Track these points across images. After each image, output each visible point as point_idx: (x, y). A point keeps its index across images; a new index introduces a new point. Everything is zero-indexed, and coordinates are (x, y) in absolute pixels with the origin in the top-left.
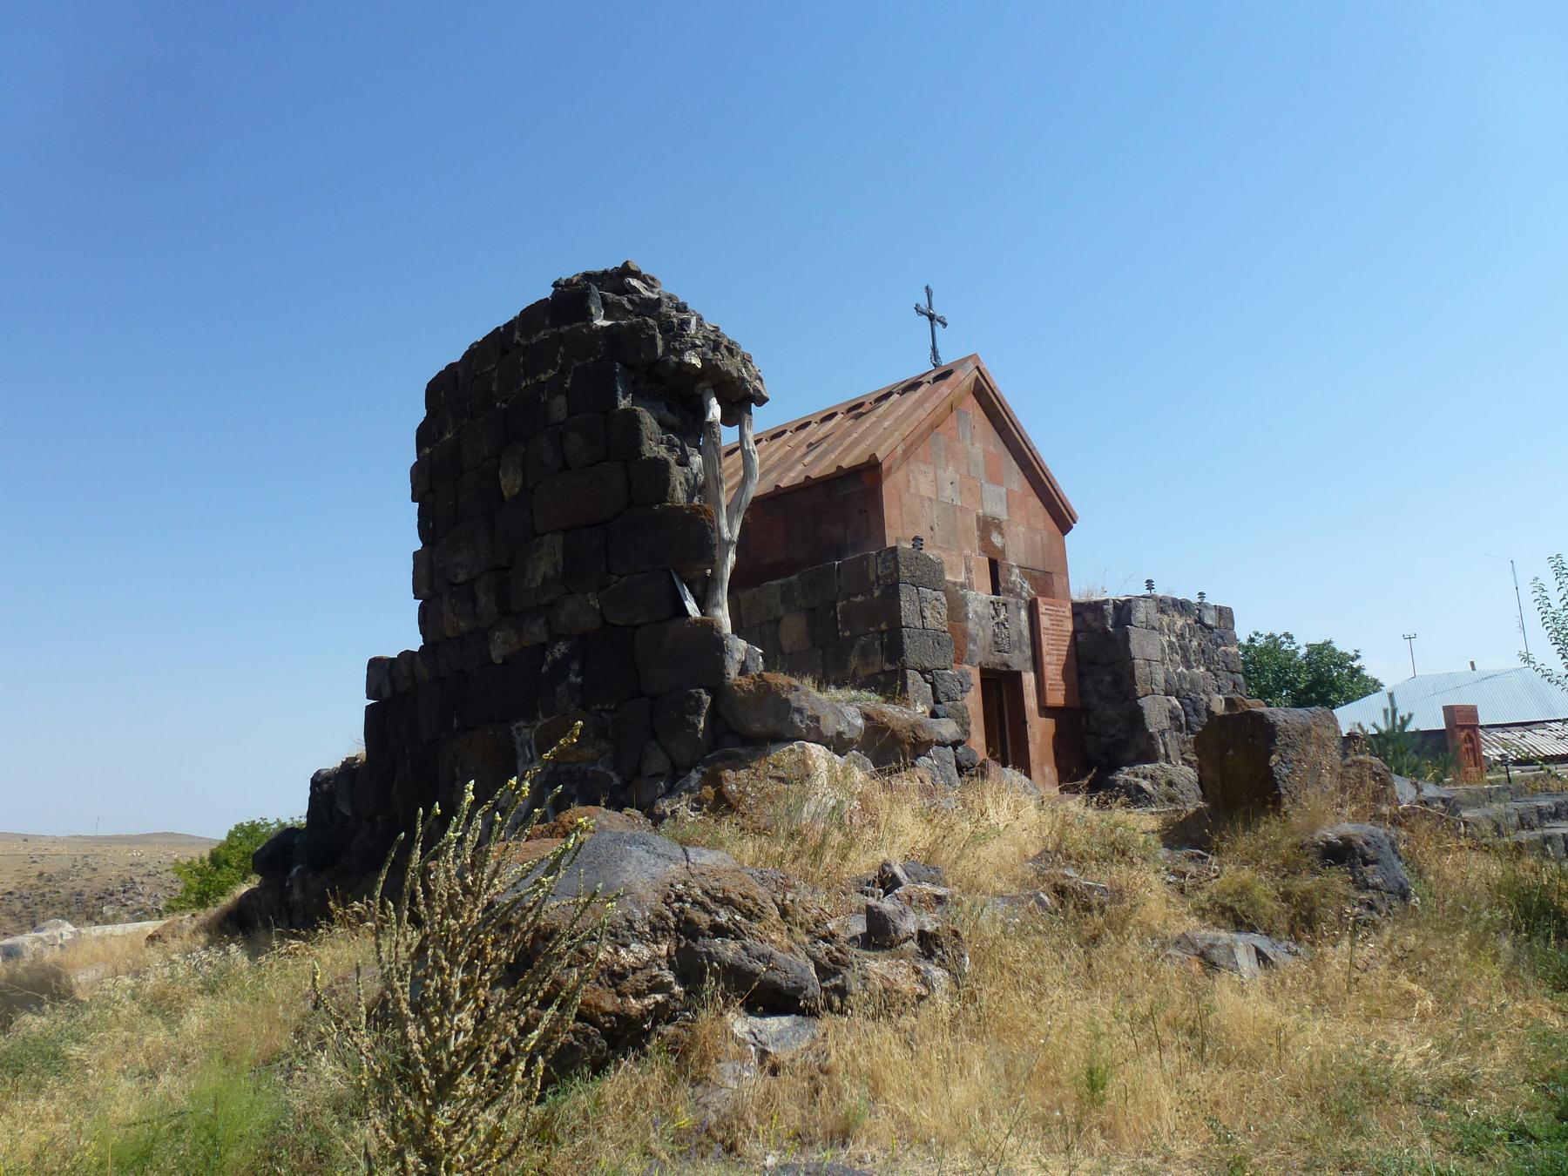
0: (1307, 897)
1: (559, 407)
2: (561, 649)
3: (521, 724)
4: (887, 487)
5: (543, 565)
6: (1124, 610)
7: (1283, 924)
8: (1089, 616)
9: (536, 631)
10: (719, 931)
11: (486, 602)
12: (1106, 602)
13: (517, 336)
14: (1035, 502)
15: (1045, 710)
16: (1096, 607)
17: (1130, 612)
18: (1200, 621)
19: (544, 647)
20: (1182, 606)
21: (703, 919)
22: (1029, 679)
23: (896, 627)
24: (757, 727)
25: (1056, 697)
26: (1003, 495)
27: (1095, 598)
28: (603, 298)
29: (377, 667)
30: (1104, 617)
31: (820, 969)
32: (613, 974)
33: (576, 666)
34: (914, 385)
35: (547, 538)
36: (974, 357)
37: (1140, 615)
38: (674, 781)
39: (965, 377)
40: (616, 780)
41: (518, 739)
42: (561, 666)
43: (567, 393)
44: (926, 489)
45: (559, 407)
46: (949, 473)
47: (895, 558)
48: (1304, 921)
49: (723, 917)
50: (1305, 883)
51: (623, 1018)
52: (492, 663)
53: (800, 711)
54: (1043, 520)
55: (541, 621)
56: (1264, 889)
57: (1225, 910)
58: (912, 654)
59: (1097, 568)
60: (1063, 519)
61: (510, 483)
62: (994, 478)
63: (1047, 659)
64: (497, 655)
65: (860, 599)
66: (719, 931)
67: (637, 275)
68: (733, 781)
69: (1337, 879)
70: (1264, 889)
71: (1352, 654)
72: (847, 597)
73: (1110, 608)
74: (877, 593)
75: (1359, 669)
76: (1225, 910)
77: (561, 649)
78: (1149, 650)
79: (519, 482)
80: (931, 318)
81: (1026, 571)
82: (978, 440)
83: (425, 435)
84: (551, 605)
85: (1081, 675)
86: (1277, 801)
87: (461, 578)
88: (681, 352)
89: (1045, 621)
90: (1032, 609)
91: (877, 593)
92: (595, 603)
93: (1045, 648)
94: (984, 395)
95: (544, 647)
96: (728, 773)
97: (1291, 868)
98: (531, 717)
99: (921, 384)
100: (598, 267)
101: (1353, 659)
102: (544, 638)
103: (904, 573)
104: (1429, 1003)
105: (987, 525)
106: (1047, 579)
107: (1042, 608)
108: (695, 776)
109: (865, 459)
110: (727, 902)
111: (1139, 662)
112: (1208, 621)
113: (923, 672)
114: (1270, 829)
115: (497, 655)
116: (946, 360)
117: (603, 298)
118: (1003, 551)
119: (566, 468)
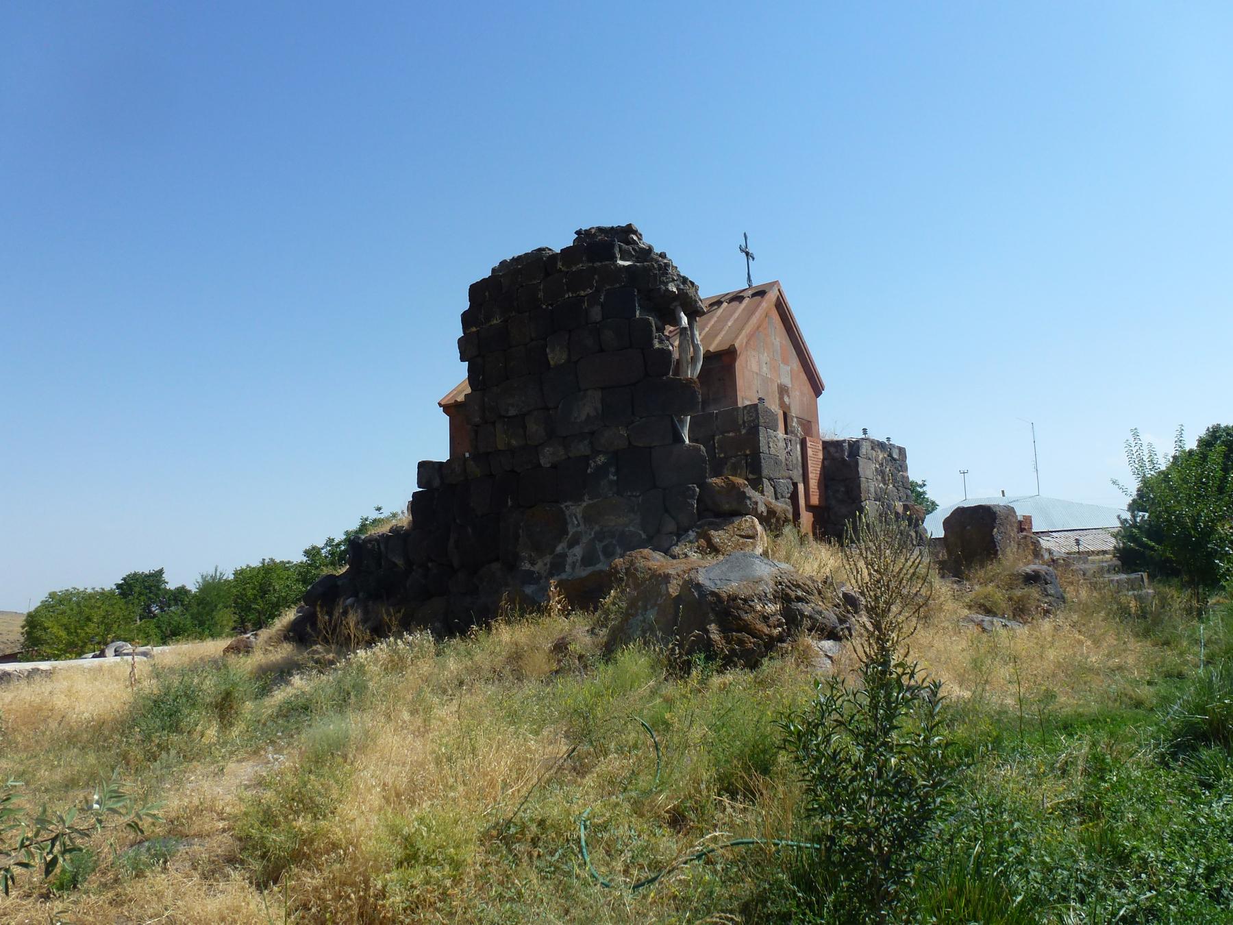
0: (1021, 599)
1: (596, 313)
2: (601, 459)
3: (568, 503)
4: (739, 364)
5: (588, 408)
6: (855, 446)
7: (1009, 613)
8: (832, 450)
9: (582, 448)
10: (799, 599)
11: (535, 428)
12: (844, 441)
13: (559, 265)
14: (803, 376)
15: (809, 507)
16: (838, 444)
17: (858, 448)
18: (890, 455)
19: (587, 458)
20: (881, 446)
21: (793, 595)
22: (801, 487)
23: (756, 453)
24: (726, 507)
25: (815, 500)
26: (789, 373)
27: (836, 438)
28: (620, 247)
29: (424, 467)
30: (843, 451)
31: (839, 619)
32: (764, 617)
33: (613, 470)
34: (737, 298)
35: (590, 392)
36: (776, 283)
37: (863, 451)
38: (680, 533)
39: (772, 296)
40: (644, 536)
41: (567, 513)
42: (602, 470)
43: (602, 305)
44: (755, 368)
45: (596, 313)
46: (765, 357)
47: (757, 410)
48: (1020, 611)
49: (800, 593)
50: (1018, 593)
51: (770, 637)
52: (540, 465)
53: (750, 498)
54: (807, 388)
55: (586, 442)
56: (999, 596)
57: (982, 606)
58: (765, 472)
59: (837, 420)
60: (817, 387)
61: (556, 356)
62: (786, 362)
63: (811, 475)
64: (545, 462)
65: (731, 434)
66: (799, 599)
67: (635, 232)
68: (718, 536)
69: (1034, 592)
70: (999, 596)
71: (920, 483)
72: (722, 433)
73: (846, 445)
74: (743, 432)
75: (924, 493)
76: (982, 606)
77: (601, 459)
78: (867, 470)
79: (565, 356)
80: (747, 254)
81: (801, 421)
82: (778, 337)
83: (467, 319)
84: (592, 433)
85: (826, 487)
86: (996, 553)
87: (512, 412)
88: (666, 284)
89: (810, 452)
90: (803, 443)
91: (743, 432)
92: (623, 432)
93: (810, 469)
94: (781, 308)
95: (587, 458)
96: (712, 532)
97: (1011, 587)
98: (578, 499)
99: (743, 298)
100: (607, 224)
101: (921, 486)
102: (588, 452)
103: (761, 420)
104: (1089, 643)
105: (783, 390)
106: (809, 425)
107: (809, 444)
108: (692, 534)
109: (725, 347)
110: (798, 586)
111: (863, 479)
112: (895, 456)
113: (770, 479)
114: (992, 568)
115: (545, 462)
116: (757, 282)
117: (620, 247)
118: (789, 407)
119: (602, 350)
